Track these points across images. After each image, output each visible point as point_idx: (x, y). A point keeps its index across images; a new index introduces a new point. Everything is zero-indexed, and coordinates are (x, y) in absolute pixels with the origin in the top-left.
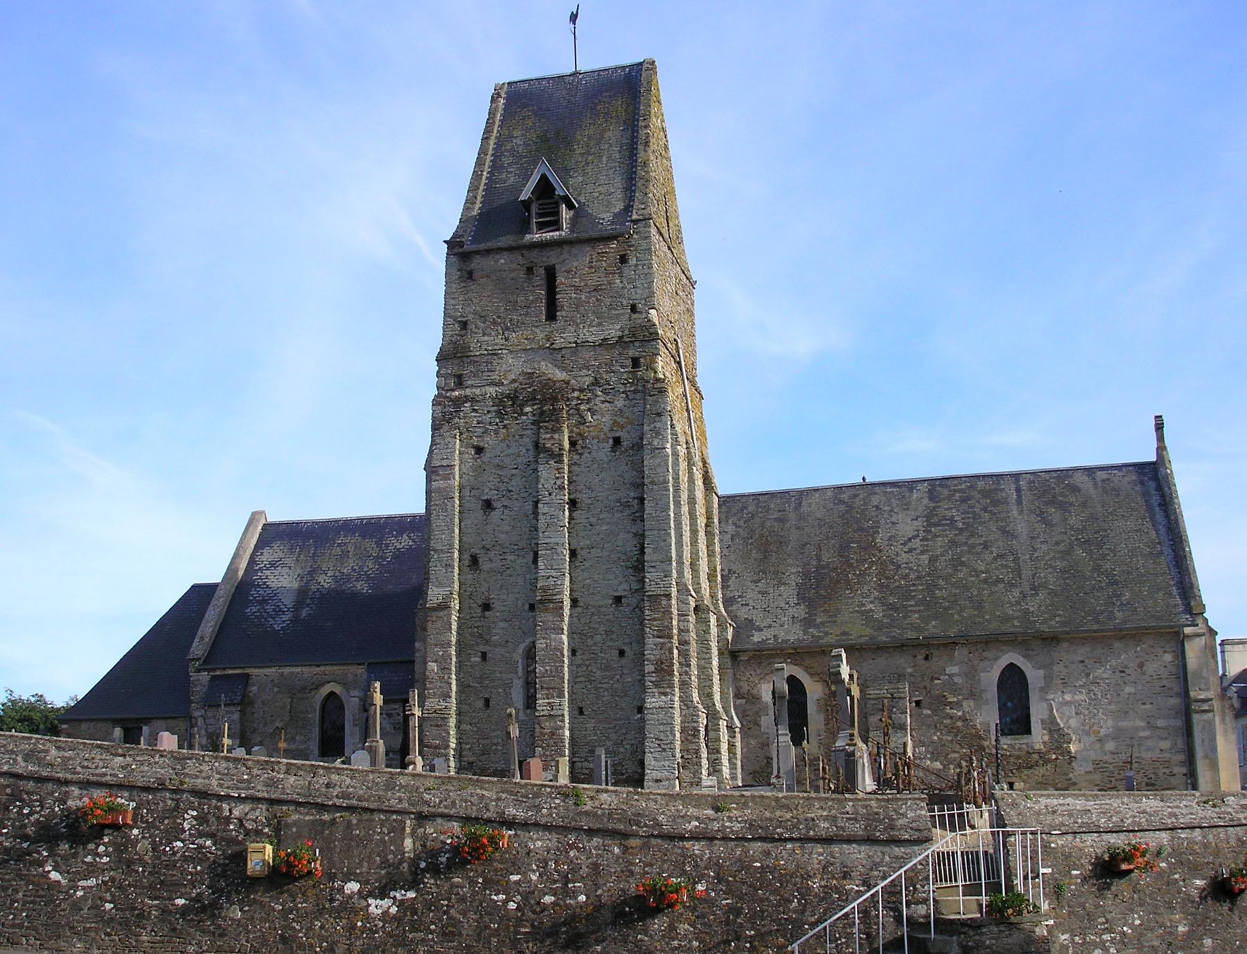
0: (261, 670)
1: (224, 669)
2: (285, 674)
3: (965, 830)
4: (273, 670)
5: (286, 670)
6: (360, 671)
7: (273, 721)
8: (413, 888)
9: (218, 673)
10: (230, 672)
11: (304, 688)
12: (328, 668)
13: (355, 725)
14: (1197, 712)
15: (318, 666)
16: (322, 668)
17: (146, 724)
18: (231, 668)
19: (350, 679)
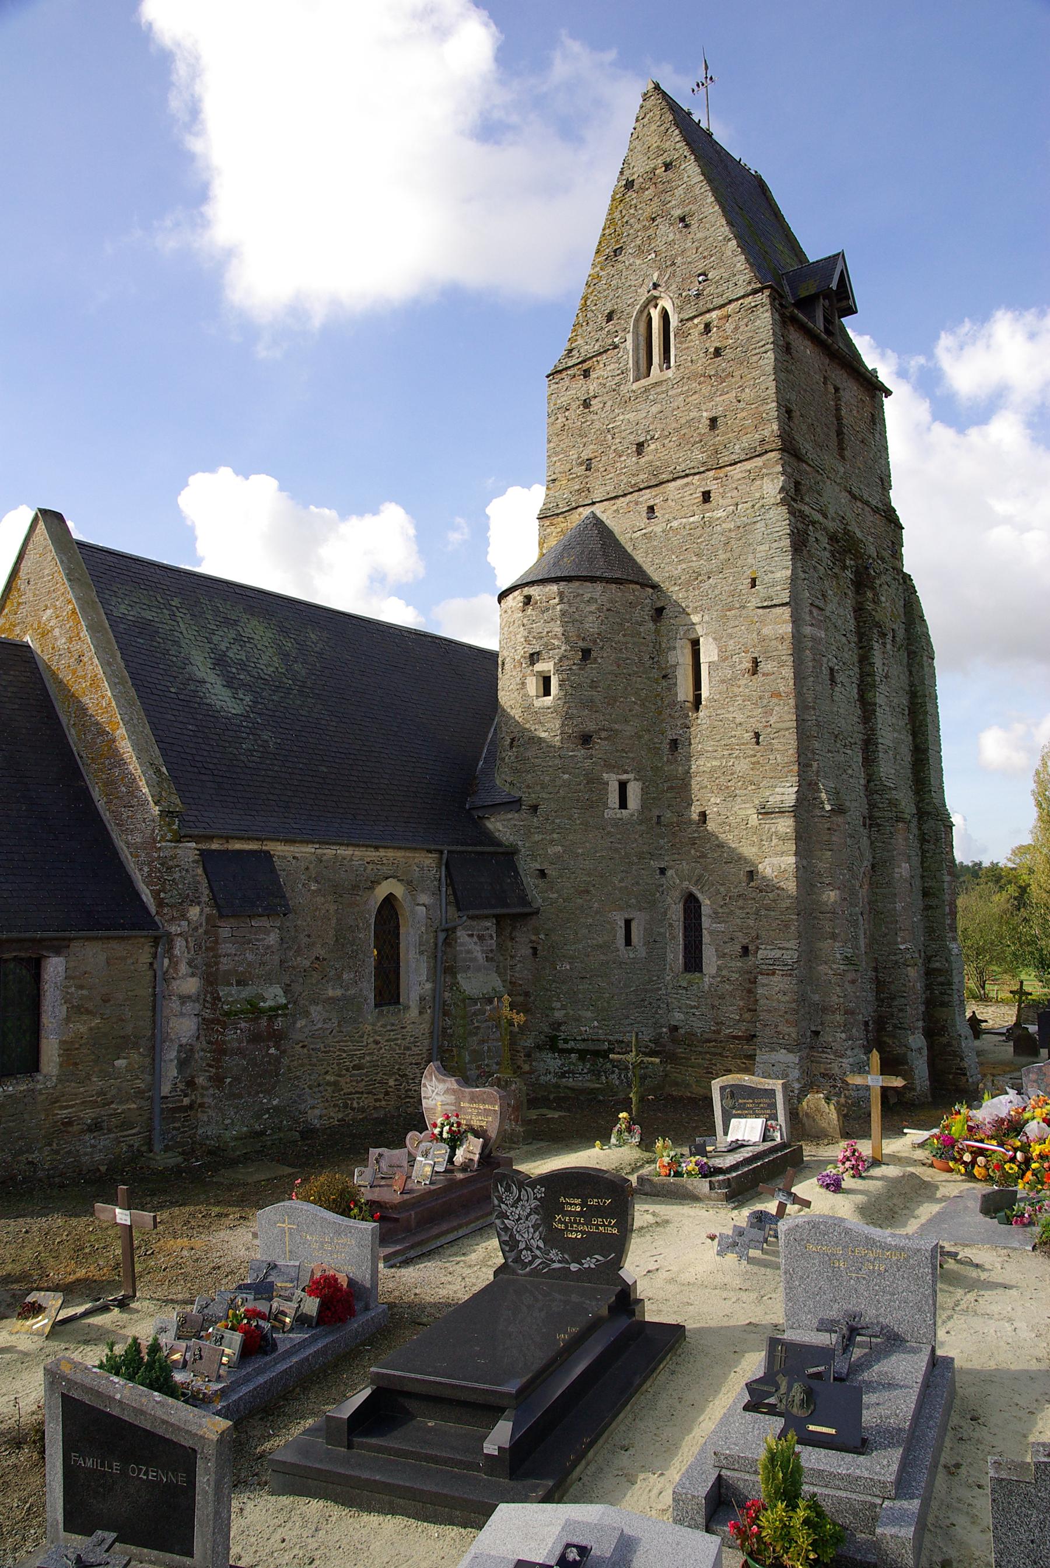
0: (287, 848)
1: (228, 839)
2: (325, 858)
3: (884, 1090)
4: (310, 849)
5: (329, 852)
6: (428, 862)
7: (310, 946)
8: (818, 901)
9: (215, 846)
10: (238, 846)
11: (355, 887)
12: (390, 853)
13: (421, 953)
14: (702, 181)
15: (377, 848)
16: (382, 853)
17: (58, 952)
18: (240, 838)
19: (417, 874)
